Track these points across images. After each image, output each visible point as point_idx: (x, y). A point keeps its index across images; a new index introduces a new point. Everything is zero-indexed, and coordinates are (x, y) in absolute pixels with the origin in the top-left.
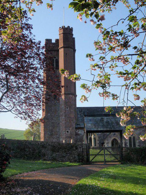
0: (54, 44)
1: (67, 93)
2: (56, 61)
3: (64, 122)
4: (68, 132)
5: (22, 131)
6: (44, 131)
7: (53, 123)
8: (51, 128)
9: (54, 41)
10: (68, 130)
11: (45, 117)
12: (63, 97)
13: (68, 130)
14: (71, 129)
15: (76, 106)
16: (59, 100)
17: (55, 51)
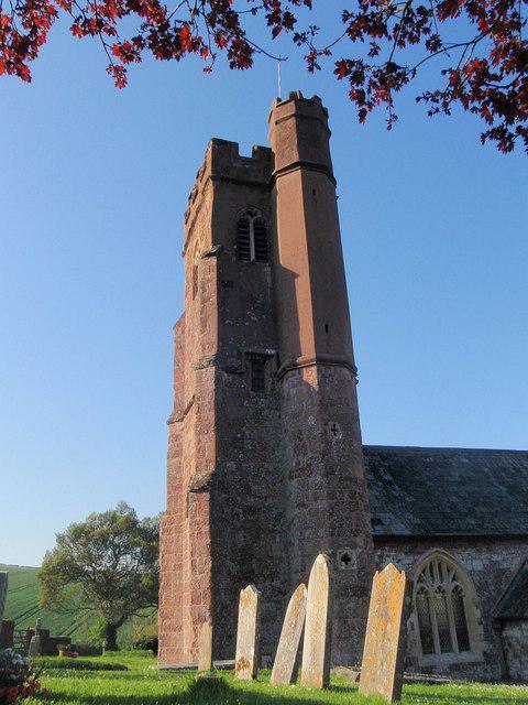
0: (246, 160)
1: (327, 356)
2: (255, 228)
3: (322, 504)
4: (346, 559)
5: (26, 571)
6: (213, 554)
7: (249, 510)
8: (240, 538)
9: (245, 152)
10: (347, 550)
11: (214, 475)
12: (311, 376)
13: (347, 550)
14: (359, 540)
15: (351, 423)
16: (278, 397)
17: (253, 185)
